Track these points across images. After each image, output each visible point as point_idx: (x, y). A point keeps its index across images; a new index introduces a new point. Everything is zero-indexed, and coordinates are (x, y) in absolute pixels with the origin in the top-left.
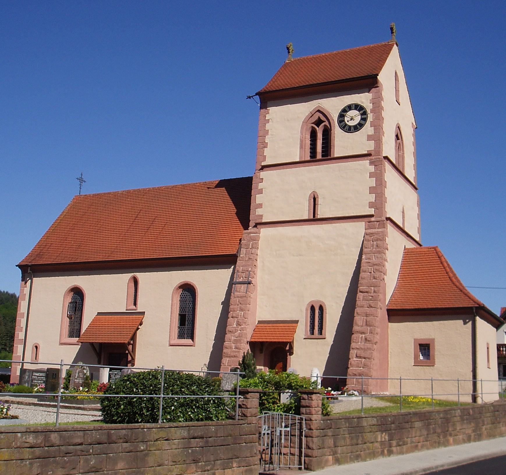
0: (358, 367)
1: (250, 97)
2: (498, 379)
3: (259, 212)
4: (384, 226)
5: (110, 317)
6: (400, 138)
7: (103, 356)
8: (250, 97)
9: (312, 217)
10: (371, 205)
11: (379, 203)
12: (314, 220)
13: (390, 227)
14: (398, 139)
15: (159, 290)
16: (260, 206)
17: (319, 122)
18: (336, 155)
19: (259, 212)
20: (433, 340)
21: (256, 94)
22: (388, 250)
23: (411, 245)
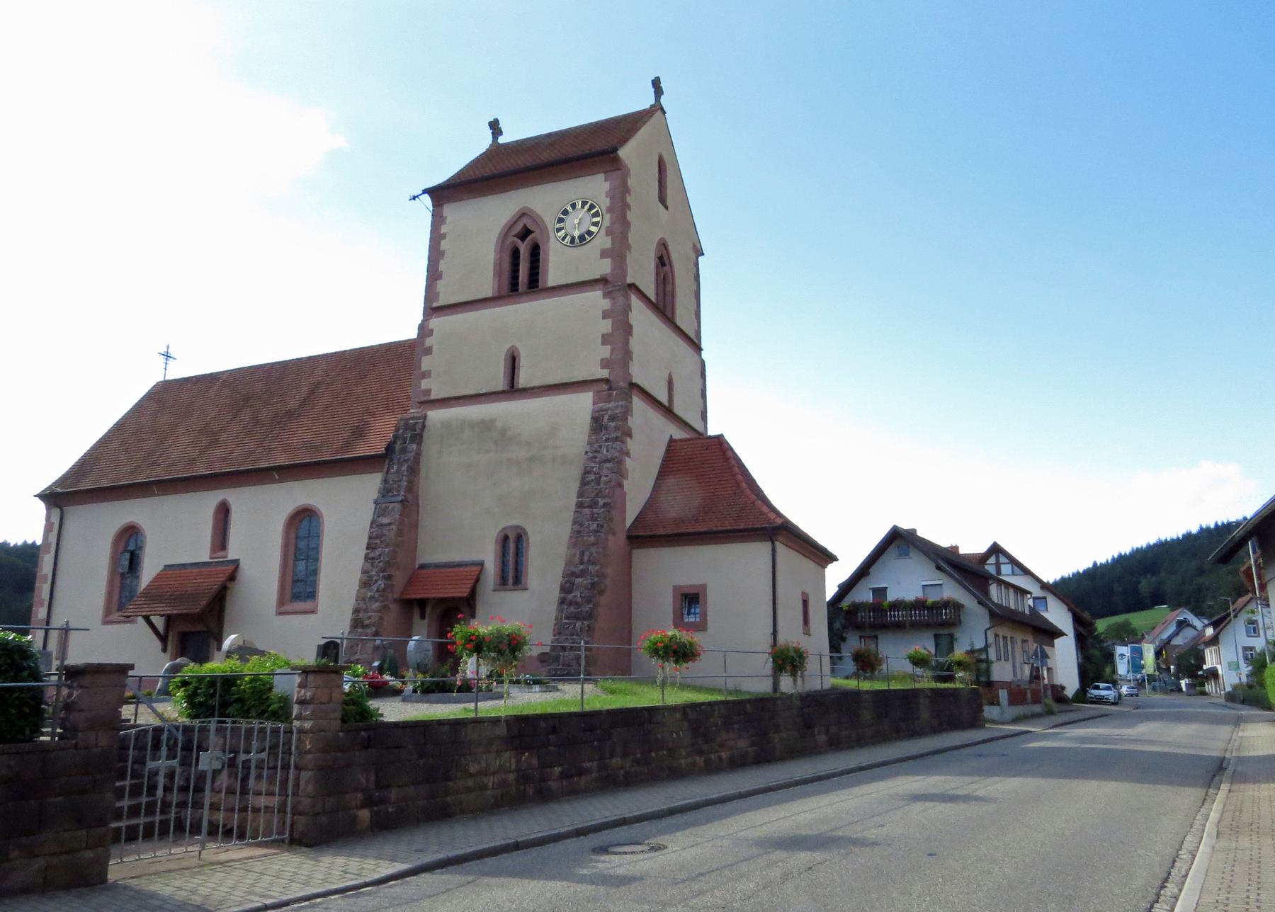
0: (587, 664)
1: (414, 198)
2: (618, 172)
3: (425, 384)
4: (628, 398)
5: (774, 816)
6: (667, 262)
7: (170, 638)
8: (414, 198)
9: (506, 388)
10: (605, 364)
11: (623, 356)
12: (513, 390)
13: (637, 403)
14: (663, 264)
15: (259, 520)
16: (425, 375)
17: (525, 234)
18: (551, 283)
19: (425, 384)
20: (704, 587)
21: (425, 191)
22: (631, 436)
23: (679, 434)
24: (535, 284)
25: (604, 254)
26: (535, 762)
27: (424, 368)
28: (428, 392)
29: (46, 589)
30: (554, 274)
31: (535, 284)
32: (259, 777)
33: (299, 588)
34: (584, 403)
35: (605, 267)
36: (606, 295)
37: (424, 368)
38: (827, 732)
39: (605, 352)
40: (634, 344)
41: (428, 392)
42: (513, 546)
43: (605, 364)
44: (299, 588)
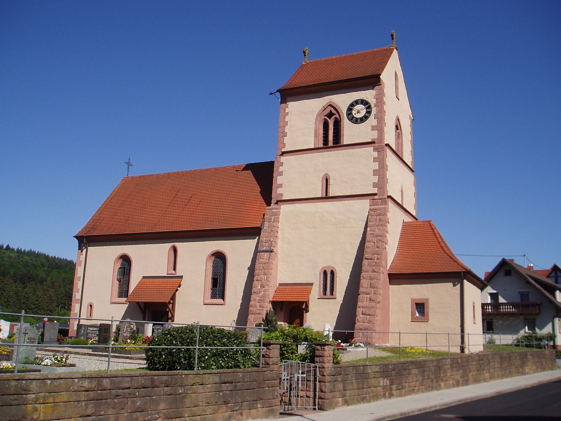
3: (280, 191)
4: (386, 203)
7: (147, 314)
11: (381, 183)
12: (327, 197)
13: (391, 204)
15: (195, 257)
16: (281, 186)
17: (330, 115)
19: (280, 191)
20: (427, 300)
21: (278, 91)
24: (337, 142)
25: (373, 128)
26: (388, 382)
27: (279, 182)
28: (281, 195)
29: (80, 287)
30: (346, 139)
31: (337, 142)
32: (303, 384)
33: (218, 287)
34: (365, 204)
35: (374, 135)
36: (375, 150)
37: (279, 182)
38: (489, 372)
39: (376, 179)
40: (389, 175)
41: (281, 195)
42: (328, 277)
43: (375, 185)
44: (218, 287)
